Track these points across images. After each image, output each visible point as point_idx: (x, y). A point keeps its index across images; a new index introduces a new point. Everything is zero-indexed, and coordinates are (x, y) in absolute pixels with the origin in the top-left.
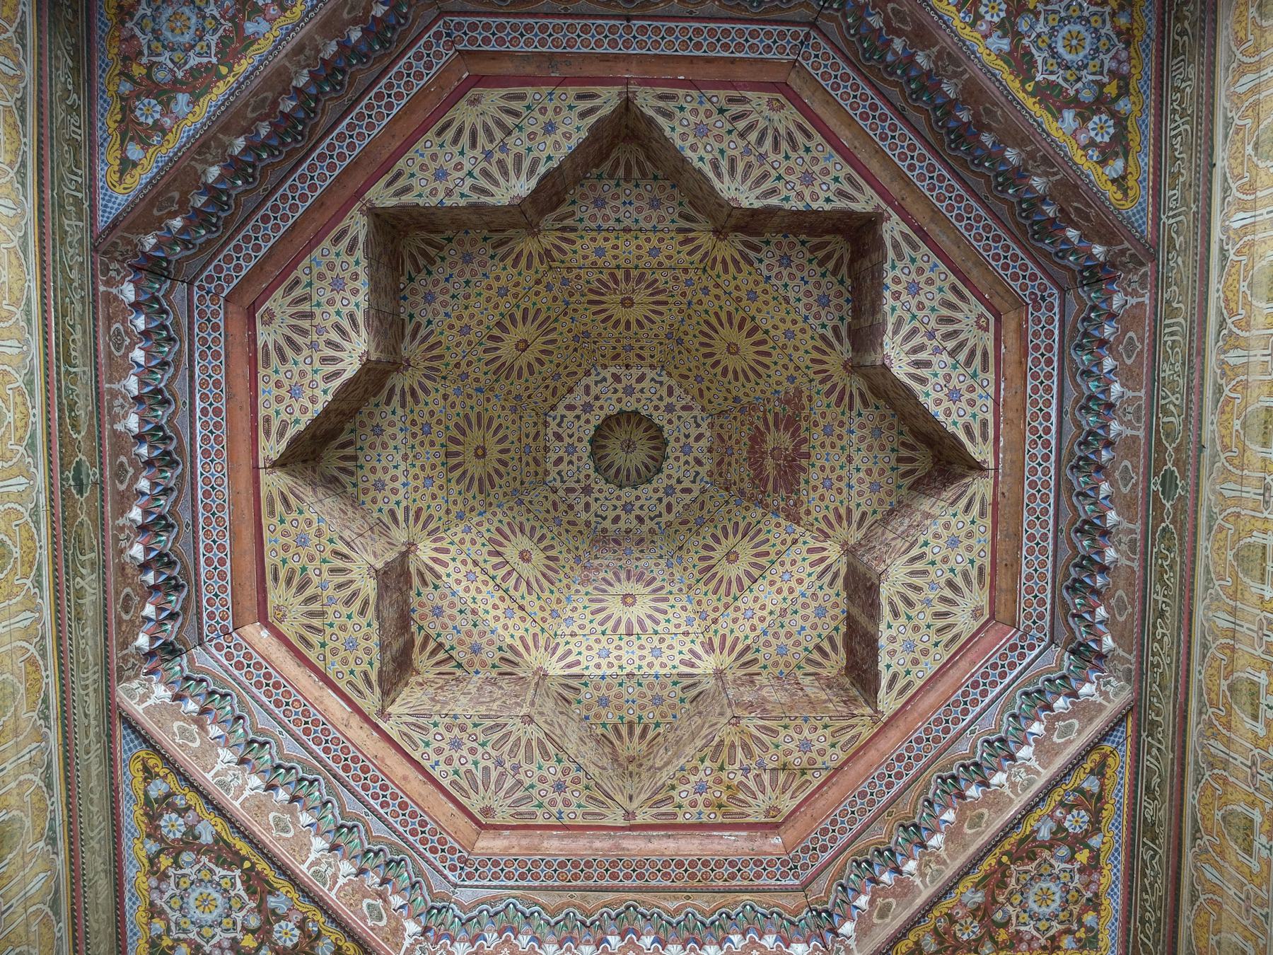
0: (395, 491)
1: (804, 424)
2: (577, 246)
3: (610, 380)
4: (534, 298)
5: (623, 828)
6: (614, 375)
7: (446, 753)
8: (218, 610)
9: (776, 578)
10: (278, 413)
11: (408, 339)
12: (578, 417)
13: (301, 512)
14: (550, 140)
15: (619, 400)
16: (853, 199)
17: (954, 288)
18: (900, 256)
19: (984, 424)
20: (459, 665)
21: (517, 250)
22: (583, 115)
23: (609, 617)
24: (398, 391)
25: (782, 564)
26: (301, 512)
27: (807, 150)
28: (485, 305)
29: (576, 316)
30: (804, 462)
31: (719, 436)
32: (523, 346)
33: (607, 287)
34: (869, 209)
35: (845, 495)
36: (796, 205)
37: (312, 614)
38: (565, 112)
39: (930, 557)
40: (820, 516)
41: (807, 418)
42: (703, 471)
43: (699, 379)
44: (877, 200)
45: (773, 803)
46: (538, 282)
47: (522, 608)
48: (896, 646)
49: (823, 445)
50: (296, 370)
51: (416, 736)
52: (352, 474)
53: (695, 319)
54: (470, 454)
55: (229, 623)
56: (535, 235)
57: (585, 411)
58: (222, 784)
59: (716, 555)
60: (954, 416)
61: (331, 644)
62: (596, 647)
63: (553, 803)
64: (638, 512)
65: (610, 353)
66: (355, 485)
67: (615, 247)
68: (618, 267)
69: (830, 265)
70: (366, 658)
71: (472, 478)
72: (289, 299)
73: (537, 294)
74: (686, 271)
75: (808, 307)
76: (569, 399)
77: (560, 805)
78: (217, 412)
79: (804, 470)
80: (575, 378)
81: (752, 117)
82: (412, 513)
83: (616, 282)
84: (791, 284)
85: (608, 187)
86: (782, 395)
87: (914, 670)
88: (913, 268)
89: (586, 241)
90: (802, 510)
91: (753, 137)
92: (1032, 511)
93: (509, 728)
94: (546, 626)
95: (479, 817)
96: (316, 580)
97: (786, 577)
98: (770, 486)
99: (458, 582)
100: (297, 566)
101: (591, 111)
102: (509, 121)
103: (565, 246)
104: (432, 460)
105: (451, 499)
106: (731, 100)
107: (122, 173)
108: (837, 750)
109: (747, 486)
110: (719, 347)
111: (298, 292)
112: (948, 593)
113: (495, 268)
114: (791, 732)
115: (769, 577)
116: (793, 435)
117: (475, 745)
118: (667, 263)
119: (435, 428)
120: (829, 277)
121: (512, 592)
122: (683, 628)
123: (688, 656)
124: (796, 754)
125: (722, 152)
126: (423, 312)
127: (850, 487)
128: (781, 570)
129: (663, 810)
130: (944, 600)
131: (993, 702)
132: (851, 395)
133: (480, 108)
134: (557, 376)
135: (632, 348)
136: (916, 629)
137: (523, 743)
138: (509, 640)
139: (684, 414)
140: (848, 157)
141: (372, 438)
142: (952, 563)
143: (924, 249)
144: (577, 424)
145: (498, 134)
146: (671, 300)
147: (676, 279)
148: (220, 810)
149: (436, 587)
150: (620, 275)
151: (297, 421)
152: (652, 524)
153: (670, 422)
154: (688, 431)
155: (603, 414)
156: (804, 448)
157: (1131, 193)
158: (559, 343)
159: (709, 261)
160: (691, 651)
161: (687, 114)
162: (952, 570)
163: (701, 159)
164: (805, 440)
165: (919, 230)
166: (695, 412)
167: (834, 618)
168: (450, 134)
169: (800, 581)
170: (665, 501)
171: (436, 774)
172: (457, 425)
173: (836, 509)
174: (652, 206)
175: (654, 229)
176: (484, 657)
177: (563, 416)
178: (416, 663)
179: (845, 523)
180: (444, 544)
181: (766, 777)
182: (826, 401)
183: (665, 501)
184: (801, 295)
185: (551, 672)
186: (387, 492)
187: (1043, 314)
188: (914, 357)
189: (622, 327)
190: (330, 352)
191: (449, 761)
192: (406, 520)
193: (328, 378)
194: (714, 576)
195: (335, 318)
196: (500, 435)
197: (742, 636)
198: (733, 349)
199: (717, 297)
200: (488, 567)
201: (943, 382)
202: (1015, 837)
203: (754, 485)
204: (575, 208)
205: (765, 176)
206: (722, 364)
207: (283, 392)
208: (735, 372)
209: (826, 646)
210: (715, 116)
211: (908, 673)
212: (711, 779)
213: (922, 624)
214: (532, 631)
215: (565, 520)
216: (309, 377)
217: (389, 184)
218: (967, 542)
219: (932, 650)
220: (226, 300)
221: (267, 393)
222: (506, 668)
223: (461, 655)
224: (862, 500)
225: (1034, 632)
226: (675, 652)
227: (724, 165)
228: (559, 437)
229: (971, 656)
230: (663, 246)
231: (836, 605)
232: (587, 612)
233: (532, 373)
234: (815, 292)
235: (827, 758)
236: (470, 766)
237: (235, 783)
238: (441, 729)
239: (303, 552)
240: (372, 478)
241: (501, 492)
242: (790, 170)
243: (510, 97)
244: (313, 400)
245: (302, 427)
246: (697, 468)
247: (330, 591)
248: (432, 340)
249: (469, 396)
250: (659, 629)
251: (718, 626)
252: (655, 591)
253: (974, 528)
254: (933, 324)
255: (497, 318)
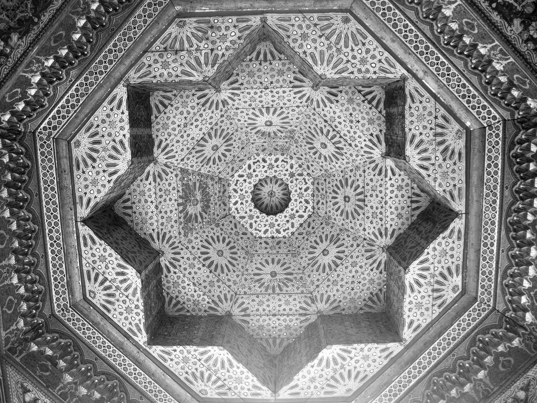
0: (392, 185)
1: (182, 220)
2: (299, 305)
3: (281, 230)
4: (320, 278)
5: (267, 12)
6: (280, 233)
7: (369, 56)
8: (494, 139)
9: (191, 141)
10: (453, 242)
11: (383, 262)
12: (297, 212)
13: (444, 191)
14: (312, 375)
15: (276, 220)
16: (163, 351)
17: (109, 311)
18: (137, 325)
19: (86, 245)
20: (360, 92)
21: (328, 305)
22: (296, 386)
23: (279, 115)
24: (389, 236)
25: (188, 149)
26: (444, 191)
27: (187, 373)
28: (344, 277)
29: (298, 266)
30: (181, 201)
31: (225, 205)
32: (325, 252)
33: (283, 283)
34: (154, 347)
35: (158, 189)
36: (191, 348)
37: (441, 134)
38: (305, 387)
39: (106, 175)
40: (170, 175)
41: (181, 223)
42: (233, 186)
43: (237, 233)
44: (151, 351)
45: (181, 30)
46: (318, 286)
47: (326, 121)
48: (120, 125)
49: (171, 211)
50: (443, 264)
51: (386, 66)
52: (414, 194)
53: (240, 267)
54: (352, 200)
55: (488, 132)
56: (319, 312)
57: (294, 215)
58: (504, 54)
59: (224, 148)
60: (101, 249)
61: (432, 118)
62: (285, 101)
63: (308, 27)
64: (265, 164)
65: (282, 245)
66: (412, 188)
67: (280, 306)
68: (278, 294)
69: (174, 301)
70: (413, 111)
71: (351, 187)
72: (444, 298)
73: (318, 280)
74: (245, 293)
75: (183, 282)
76: (302, 220)
77: (304, 25)
78: (485, 245)
79: (180, 197)
80: (299, 231)
81: (214, 386)
82: (383, 173)
83: (279, 286)
84: (193, 292)
85: (284, 334)
86: (194, 232)
87: (108, 111)
88: (130, 320)
89: (294, 309)
90: (180, 176)
91: (214, 378)
92: (54, 203)
93: (334, 72)
94: (313, 111)
95: (351, 17)
96: (438, 154)
97: (185, 143)
98: (198, 185)
99: (360, 137)
100: (448, 161)
101: (292, 388)
102: (332, 382)
103: (305, 306)
104: (372, 199)
105: (363, 178)
106: (225, 394)
107: (529, 385)
108: (147, 63)
109: (210, 183)
110: (227, 254)
111: (439, 302)
112: (95, 155)
113: (339, 296)
114: (174, 73)
115: (195, 141)
116: (187, 213)
117: (353, 61)
118: (254, 297)
119: (370, 215)
120: (174, 296)
121: (331, 129)
122: (239, 111)
123: (236, 98)
124: (170, 60)
125: (228, 371)
126: (375, 275)
127: (155, 193)
128: (188, 146)
129: (244, 24)
130: (97, 151)
131: (62, 97)
132: (158, 239)
133: (346, 388)
134: (308, 233)
135: (271, 248)
136: (110, 135)
137: (325, 63)
138: (333, 106)
139: (244, 215)
140: (167, 370)
141: (403, 212)
142: (94, 171)
143: (125, 329)
144: (298, 208)
145: (338, 376)
146: (252, 276)
147: (250, 289)
148: (507, 41)
149: (372, 135)
150: (277, 290)
151: (444, 238)
152: (258, 158)
153: (251, 210)
154: (241, 206)
155: (285, 213)
156: (181, 208)
157: (19, 385)
158: (307, 251)
159: (234, 300)
160: (234, 100)
161: (246, 387)
162: (94, 167)
163: (238, 368)
164: (181, 212)
165: (128, 337)
166: (238, 215)
167: (158, 123)
168: (361, 376)
169: (178, 142)
170: (252, 170)
171: (376, 43)
172: (359, 215)
173: (162, 180)
174: (263, 326)
175: (261, 316)
176: (346, 97)
177: (305, 212)
178: (383, 92)
179: (156, 174)
180: (367, 155)
181: (186, 45)
182: (172, 234)
183: (252, 170)
184: (187, 287)
185: (310, 89)
186: (396, 185)
187: (62, 303)
188: (125, 277)
189: (276, 260)
190: (425, 273)
191: (368, 51)
192: (386, 170)
193: (426, 260)
194: (224, 138)
195: (421, 290)
196: (337, 206)
197: (207, 111)
198: (220, 253)
199: (229, 280)
200: (343, 143)
201: (109, 265)
202: (32, 35)
203: (206, 184)
204: (300, 325)
205: (207, 361)
206: (225, 244)
207: (450, 253)
208: (219, 241)
209: (161, 108)
210: (232, 387)
211: (112, 110)
212: (218, 44)
213: (106, 137)
214: (320, 109)
215: (303, 161)
216: (436, 261)
217: (392, 353)
218: (87, 183)
219: (100, 122)
220: (476, 299)
221: (459, 252)
222: (334, 91)
223: (359, 98)
224: (148, 186)
225: (45, 137)
226: (243, 100)
227: (227, 365)
228: (307, 202)
229: (78, 121)
230: (257, 307)
231: (158, 130)
232: (291, 117)
233: (321, 237)
234: (180, 289)
235: (153, 58)
236: (356, 48)
237: (495, 52)
238: (372, 70)
239: (444, 169)
240: (403, 192)
241: (336, 177)
242: (195, 364)
243: (332, 392)
244: (435, 249)
245: (441, 235)
246: (236, 187)
247: (431, 148)
248: (371, 261)
249: (352, 228)
250: (252, 111)
251: (220, 114)
252: (255, 128)
253: (85, 190)
254: (117, 294)
255: (338, 269)
